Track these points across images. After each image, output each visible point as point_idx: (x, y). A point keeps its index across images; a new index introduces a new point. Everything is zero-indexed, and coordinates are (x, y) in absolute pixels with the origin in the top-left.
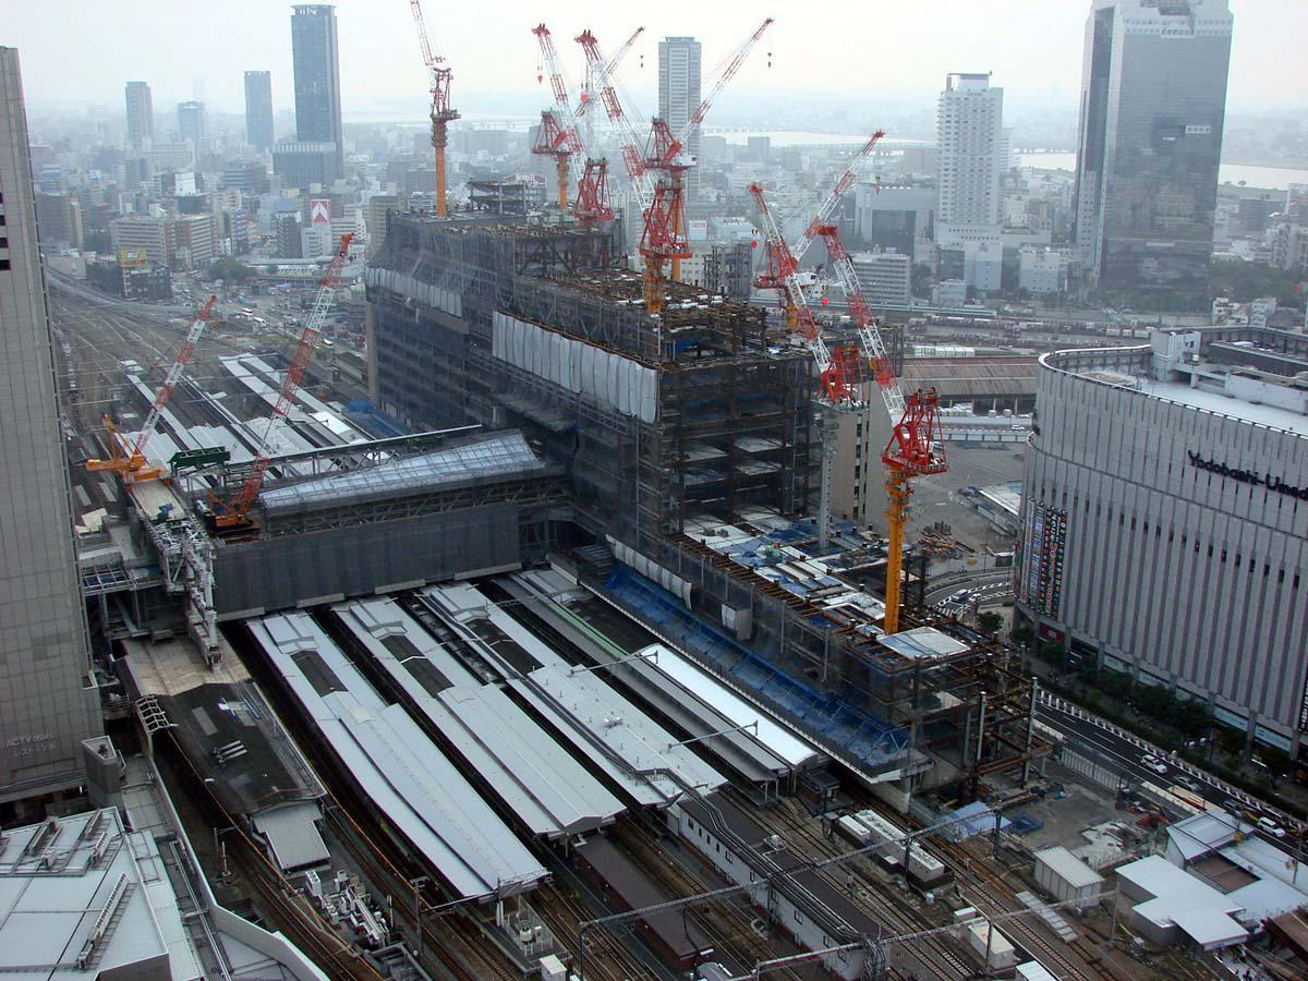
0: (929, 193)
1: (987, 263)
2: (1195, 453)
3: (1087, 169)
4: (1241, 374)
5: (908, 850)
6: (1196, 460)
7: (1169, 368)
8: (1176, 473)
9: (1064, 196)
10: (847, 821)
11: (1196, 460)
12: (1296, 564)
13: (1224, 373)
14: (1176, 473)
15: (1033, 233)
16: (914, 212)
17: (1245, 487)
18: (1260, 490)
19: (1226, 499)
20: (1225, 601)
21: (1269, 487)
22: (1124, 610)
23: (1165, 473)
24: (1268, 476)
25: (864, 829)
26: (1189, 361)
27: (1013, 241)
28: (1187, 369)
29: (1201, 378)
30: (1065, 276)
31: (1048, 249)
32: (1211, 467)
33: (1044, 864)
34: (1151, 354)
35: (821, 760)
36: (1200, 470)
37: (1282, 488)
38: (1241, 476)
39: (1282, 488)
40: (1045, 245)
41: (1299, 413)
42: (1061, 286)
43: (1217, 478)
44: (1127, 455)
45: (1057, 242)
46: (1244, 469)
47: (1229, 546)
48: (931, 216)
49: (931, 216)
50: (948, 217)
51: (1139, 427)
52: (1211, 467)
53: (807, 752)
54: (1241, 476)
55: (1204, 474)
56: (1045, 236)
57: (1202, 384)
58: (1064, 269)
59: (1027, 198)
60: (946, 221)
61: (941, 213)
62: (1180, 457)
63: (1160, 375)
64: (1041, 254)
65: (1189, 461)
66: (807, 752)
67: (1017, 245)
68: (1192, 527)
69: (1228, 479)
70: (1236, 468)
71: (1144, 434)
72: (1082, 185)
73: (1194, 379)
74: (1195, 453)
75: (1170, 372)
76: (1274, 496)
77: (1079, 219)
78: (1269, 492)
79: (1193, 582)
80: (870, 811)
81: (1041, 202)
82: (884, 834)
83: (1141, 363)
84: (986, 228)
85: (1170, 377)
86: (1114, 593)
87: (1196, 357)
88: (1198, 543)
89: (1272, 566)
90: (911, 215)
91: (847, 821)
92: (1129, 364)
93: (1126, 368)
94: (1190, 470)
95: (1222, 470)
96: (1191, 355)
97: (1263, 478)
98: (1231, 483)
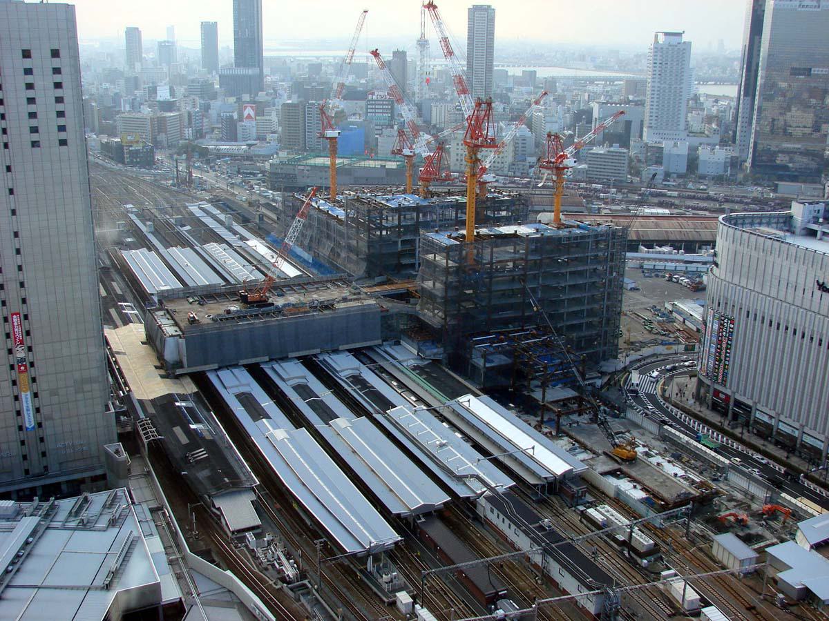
2: (821, 282)
5: (632, 532)
8: (808, 295)
10: (591, 511)
15: (708, 136)
25: (603, 517)
26: (816, 222)
27: (695, 141)
28: (815, 227)
30: (728, 165)
31: (717, 147)
36: (824, 293)
45: (723, 143)
58: (729, 160)
62: (811, 284)
63: (798, 231)
72: (741, 106)
73: (819, 234)
74: (821, 282)
75: (803, 229)
77: (738, 128)
80: (606, 506)
87: (821, 220)
91: (591, 511)
92: (777, 223)
93: (774, 225)
94: (818, 293)
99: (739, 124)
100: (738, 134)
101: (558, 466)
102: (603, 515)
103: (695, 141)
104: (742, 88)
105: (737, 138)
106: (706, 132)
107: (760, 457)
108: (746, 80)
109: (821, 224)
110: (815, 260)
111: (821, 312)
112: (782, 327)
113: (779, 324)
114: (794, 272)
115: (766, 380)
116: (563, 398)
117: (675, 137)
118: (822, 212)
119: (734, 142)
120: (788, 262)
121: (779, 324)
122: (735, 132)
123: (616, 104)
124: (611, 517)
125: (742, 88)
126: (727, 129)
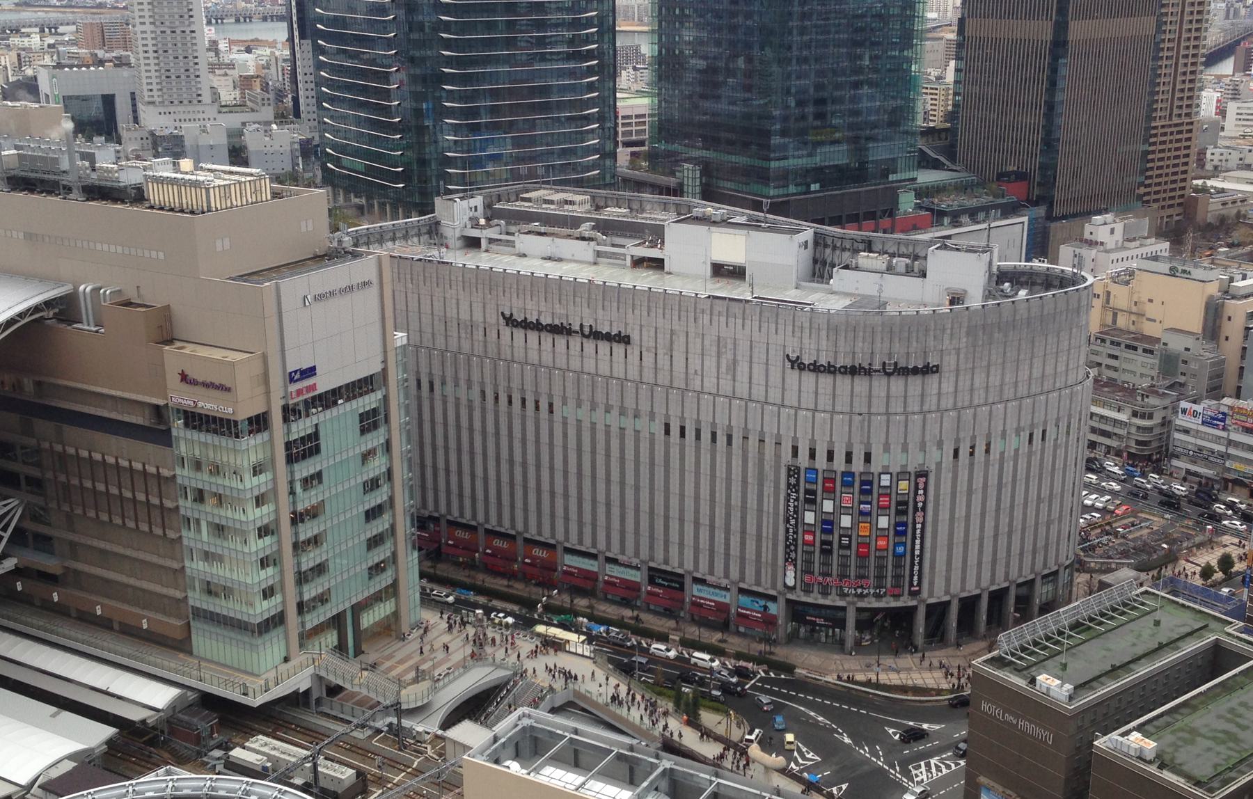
0: (125, 72)
1: (212, 147)
2: (507, 313)
3: (302, 37)
4: (529, 232)
5: (315, 766)
6: (510, 321)
7: (458, 234)
8: (493, 335)
9: (273, 69)
10: (237, 753)
11: (797, 364)
12: (695, 416)
13: (513, 234)
14: (493, 335)
15: (253, 110)
16: (113, 96)
17: (561, 341)
18: (575, 342)
19: (544, 354)
20: (630, 466)
21: (584, 335)
22: (727, 540)
23: (481, 338)
24: (581, 325)
25: (260, 757)
26: (476, 225)
27: (234, 120)
28: (475, 233)
29: (491, 241)
30: (298, 154)
31: (274, 126)
32: (526, 325)
33: (455, 742)
34: (438, 223)
35: (191, 696)
36: (515, 330)
37: (596, 335)
38: (556, 330)
39: (596, 335)
40: (268, 123)
41: (589, 263)
42: (295, 164)
43: (533, 336)
44: (439, 327)
45: (281, 118)
46: (557, 322)
47: (735, 430)
48: (133, 99)
49: (133, 99)
50: (157, 99)
51: (448, 296)
52: (526, 325)
53: (173, 692)
54: (556, 330)
55: (519, 334)
56: (268, 113)
57: (494, 247)
58: (297, 146)
59: (235, 73)
60: (153, 103)
61: (146, 93)
62: (492, 318)
63: (451, 242)
64: (268, 132)
65: (502, 320)
66: (173, 692)
67: (239, 126)
68: (722, 421)
69: (543, 335)
70: (549, 322)
71: (454, 301)
72: (298, 55)
73: (484, 243)
74: (507, 313)
75: (459, 239)
76: (590, 345)
77: (301, 93)
78: (585, 340)
79: (565, 448)
80: (260, 737)
81: (252, 77)
82: (282, 756)
83: (429, 233)
84: (200, 108)
85: (459, 243)
86: (566, 487)
87: (482, 222)
88: (537, 402)
89: (836, 450)
90: (109, 101)
91: (237, 753)
92: (419, 235)
93: (415, 239)
94: (506, 332)
95: (538, 327)
96: (477, 219)
97: (577, 328)
98: (547, 338)
99: (300, 85)
100: (302, 101)
101: (159, 696)
102: (258, 752)
103: (234, 120)
104: (295, 26)
105: (302, 108)
106: (248, 103)
107: (707, 657)
108: (298, 19)
109: (483, 228)
110: (521, 287)
111: (803, 405)
112: (706, 436)
113: (683, 429)
114: (464, 307)
115: (454, 479)
116: (457, 682)
117: (201, 116)
118: (480, 209)
119: (297, 114)
120: (454, 292)
121: (683, 429)
122: (296, 100)
123: (88, 67)
124: (273, 753)
125: (295, 26)
126: (280, 95)
